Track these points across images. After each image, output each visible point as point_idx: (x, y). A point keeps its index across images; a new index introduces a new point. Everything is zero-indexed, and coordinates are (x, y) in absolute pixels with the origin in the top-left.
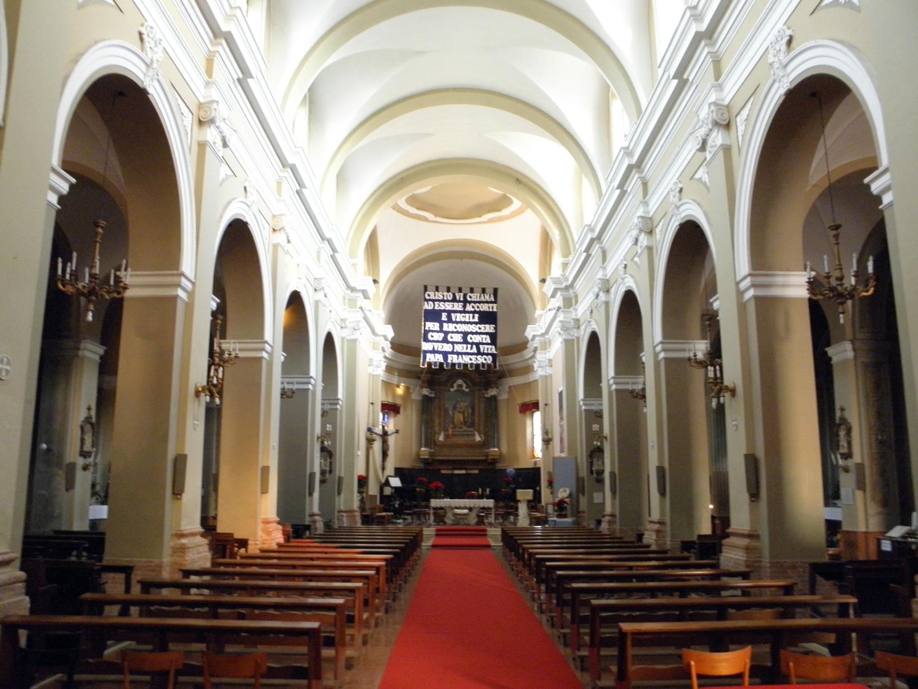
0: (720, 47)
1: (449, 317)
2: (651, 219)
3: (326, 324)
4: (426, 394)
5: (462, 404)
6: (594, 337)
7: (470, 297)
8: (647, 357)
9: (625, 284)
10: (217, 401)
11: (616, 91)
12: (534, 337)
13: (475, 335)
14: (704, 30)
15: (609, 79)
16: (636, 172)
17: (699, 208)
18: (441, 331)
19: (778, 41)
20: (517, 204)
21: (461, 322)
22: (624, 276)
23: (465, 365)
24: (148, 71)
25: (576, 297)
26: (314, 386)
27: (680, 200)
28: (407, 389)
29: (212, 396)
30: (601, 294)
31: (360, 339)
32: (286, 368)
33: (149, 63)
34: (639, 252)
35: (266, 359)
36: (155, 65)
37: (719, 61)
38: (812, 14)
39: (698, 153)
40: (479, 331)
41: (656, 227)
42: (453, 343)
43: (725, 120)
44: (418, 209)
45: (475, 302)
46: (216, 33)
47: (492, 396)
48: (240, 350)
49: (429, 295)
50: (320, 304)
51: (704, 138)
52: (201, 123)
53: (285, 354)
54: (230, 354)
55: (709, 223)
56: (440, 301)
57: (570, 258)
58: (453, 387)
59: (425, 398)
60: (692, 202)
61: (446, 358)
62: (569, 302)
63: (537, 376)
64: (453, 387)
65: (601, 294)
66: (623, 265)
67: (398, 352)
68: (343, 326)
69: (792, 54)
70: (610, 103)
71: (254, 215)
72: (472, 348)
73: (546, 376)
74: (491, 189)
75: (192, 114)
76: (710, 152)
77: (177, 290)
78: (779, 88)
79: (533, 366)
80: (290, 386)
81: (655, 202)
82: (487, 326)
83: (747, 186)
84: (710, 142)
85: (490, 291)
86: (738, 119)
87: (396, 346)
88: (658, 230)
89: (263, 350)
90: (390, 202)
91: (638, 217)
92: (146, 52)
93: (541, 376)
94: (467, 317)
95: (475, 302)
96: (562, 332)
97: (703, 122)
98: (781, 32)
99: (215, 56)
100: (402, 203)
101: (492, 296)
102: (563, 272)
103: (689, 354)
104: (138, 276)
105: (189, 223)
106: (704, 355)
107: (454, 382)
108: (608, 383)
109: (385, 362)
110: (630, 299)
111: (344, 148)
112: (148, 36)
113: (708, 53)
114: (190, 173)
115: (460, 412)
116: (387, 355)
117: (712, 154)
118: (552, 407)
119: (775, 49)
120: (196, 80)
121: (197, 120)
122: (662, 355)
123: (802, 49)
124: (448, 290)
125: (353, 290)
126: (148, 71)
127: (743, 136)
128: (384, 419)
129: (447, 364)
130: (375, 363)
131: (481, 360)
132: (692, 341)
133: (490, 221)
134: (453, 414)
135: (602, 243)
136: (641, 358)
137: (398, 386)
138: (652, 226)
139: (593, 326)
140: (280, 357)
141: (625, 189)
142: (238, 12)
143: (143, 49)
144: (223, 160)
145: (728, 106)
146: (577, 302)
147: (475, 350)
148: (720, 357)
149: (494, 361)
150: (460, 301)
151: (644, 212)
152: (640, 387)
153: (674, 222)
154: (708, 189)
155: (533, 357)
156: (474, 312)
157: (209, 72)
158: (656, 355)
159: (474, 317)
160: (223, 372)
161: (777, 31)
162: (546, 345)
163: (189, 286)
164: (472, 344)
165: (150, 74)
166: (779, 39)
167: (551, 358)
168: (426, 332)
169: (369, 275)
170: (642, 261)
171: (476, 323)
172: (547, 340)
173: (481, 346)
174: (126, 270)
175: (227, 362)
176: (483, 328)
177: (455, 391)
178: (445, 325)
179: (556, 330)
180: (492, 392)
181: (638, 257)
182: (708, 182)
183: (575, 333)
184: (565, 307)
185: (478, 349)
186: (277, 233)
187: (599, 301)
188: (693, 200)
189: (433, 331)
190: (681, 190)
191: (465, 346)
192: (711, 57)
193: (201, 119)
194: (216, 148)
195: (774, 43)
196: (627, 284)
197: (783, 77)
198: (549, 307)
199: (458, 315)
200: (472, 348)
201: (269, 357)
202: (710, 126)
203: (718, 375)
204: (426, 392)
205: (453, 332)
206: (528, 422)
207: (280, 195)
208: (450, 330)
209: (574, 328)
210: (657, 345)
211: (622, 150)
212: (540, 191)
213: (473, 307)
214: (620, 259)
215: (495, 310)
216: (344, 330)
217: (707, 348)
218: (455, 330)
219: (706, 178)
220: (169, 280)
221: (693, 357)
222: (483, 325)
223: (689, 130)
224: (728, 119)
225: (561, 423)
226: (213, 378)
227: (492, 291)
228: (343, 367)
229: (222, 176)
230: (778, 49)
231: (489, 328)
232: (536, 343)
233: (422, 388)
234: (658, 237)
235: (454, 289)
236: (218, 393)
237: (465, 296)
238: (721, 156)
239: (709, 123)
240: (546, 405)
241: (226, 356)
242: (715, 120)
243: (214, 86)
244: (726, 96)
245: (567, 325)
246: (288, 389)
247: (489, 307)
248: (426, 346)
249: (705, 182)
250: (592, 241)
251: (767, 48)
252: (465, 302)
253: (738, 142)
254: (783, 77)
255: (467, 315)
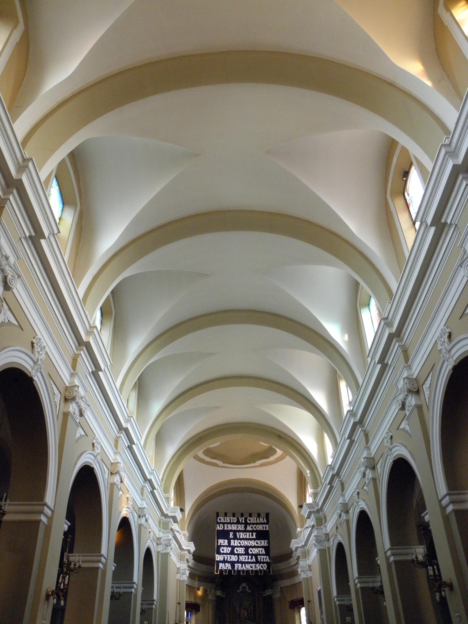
0: (405, 342)
1: (235, 536)
2: (373, 458)
3: (147, 541)
4: (219, 594)
5: (246, 602)
6: (340, 547)
7: (250, 520)
8: (381, 560)
9: (359, 506)
10: (62, 603)
11: (342, 374)
12: (297, 548)
13: (254, 549)
14: (394, 332)
15: (336, 367)
16: (360, 427)
17: (406, 449)
18: (229, 545)
19: (443, 336)
20: (279, 452)
21: (243, 539)
22: (357, 500)
23: (248, 571)
24: (34, 366)
25: (325, 517)
26: (136, 590)
27: (392, 444)
28: (205, 591)
29: (59, 600)
30: (343, 514)
31: (171, 553)
32: (116, 576)
33: (36, 361)
34: (367, 482)
35: (101, 569)
36: (39, 362)
37: (406, 351)
38: (460, 318)
39: (400, 411)
40: (256, 545)
41: (377, 464)
42: (238, 555)
43: (415, 388)
44: (211, 458)
45: (253, 524)
46: (80, 342)
47: (268, 595)
48: (82, 562)
49: (220, 520)
50: (142, 527)
51: (403, 401)
52: (66, 400)
53: (115, 565)
54: (75, 565)
55: (414, 459)
56: (228, 523)
57: (319, 489)
58: (239, 589)
59: (219, 599)
60: (400, 445)
61: (233, 566)
62: (321, 521)
63: (301, 578)
64: (239, 589)
65: (343, 514)
66: (357, 493)
67: (197, 562)
68: (158, 543)
69: (453, 343)
70: (338, 381)
71: (98, 463)
72: (252, 558)
73: (307, 579)
74: (261, 443)
75: (61, 394)
76: (408, 410)
77: (41, 516)
78: (448, 365)
79: (298, 571)
80: (118, 590)
81: (374, 447)
82: (263, 541)
83: (436, 438)
84: (407, 404)
85: (263, 515)
86: (424, 387)
87: (197, 557)
88: (379, 466)
89: (100, 561)
90: (192, 454)
91: (364, 458)
92: (35, 354)
93: (304, 579)
94: (248, 535)
95: (253, 524)
96: (317, 544)
97: (401, 390)
98: (443, 330)
99: (79, 357)
100: (200, 454)
101: (265, 519)
102: (315, 499)
103: (412, 557)
104: (14, 505)
105: (53, 478)
106: (423, 557)
107: (240, 585)
108: (354, 583)
109: (188, 570)
110: (363, 516)
111: (162, 417)
112: (37, 344)
113: (399, 346)
114: (57, 435)
115: (245, 609)
116: (190, 565)
117: (410, 411)
118: (314, 604)
119: (441, 341)
120: (65, 373)
121: (64, 397)
122: (392, 559)
123: (461, 339)
124: (234, 516)
125: (166, 516)
126: (34, 366)
127: (429, 398)
128: (187, 616)
129: (234, 571)
130: (181, 571)
131: (259, 567)
132: (413, 547)
133: (262, 465)
134: (240, 610)
135: (340, 477)
136: (377, 561)
137: (198, 589)
138: (374, 463)
139: (339, 539)
140: (112, 567)
141: (353, 438)
142: (95, 331)
143: (33, 352)
144: (79, 425)
145: (416, 379)
146: (326, 521)
147: (254, 560)
148: (436, 558)
149: (268, 568)
150: (242, 524)
151: (367, 454)
152: (379, 584)
153: (389, 460)
154: (410, 435)
155: (297, 563)
156: (252, 531)
157: (74, 367)
158: (387, 559)
159: (252, 535)
160: (69, 578)
161: (440, 330)
162: (306, 554)
163: (49, 512)
164: (252, 555)
165: (35, 368)
166: (443, 335)
167: (310, 564)
168: (219, 547)
169: (178, 506)
170: (369, 488)
171: (254, 539)
172: (306, 550)
173: (258, 557)
174: (5, 501)
175: (73, 571)
176: (259, 543)
177: (241, 592)
178: (232, 541)
179: (312, 542)
180: (268, 592)
181: (367, 486)
182: (409, 431)
183: (326, 544)
184: (317, 526)
185: (256, 558)
186: (113, 476)
187: (341, 520)
188: (401, 444)
189: (224, 546)
190: (391, 437)
191: (247, 557)
192: (401, 349)
193: (67, 397)
194: (75, 416)
195: (440, 338)
196: (360, 506)
197: (449, 358)
198: (307, 525)
199: (241, 533)
200: (252, 558)
201: (104, 567)
202: (406, 393)
203: (437, 573)
204: (219, 593)
205: (238, 547)
206: (297, 617)
207: (117, 449)
208: (236, 545)
209: (326, 540)
210: (388, 551)
211: (349, 413)
212: (295, 444)
213: (252, 528)
214: (354, 488)
215: (267, 529)
216: (160, 546)
217: (425, 551)
218: (239, 545)
219: (407, 428)
220: (95, 558)
221: (415, 559)
222: (259, 541)
223: (392, 397)
224: (417, 387)
225: (322, 616)
226: (61, 584)
227: (265, 515)
228: (158, 575)
229: (78, 435)
230: (443, 340)
231: (264, 543)
232: (298, 553)
233: (216, 590)
234: (379, 471)
235: (238, 515)
236: (63, 596)
237: (246, 519)
238: (416, 412)
239: (405, 391)
240: (309, 601)
241: (72, 566)
242: (409, 389)
243: (77, 376)
244: (414, 373)
245: (320, 538)
246: (116, 592)
247: (263, 527)
248: (219, 558)
249: (407, 431)
250: (333, 476)
251: (436, 340)
252: (246, 524)
253: (426, 402)
254: (449, 358)
255: (248, 534)
